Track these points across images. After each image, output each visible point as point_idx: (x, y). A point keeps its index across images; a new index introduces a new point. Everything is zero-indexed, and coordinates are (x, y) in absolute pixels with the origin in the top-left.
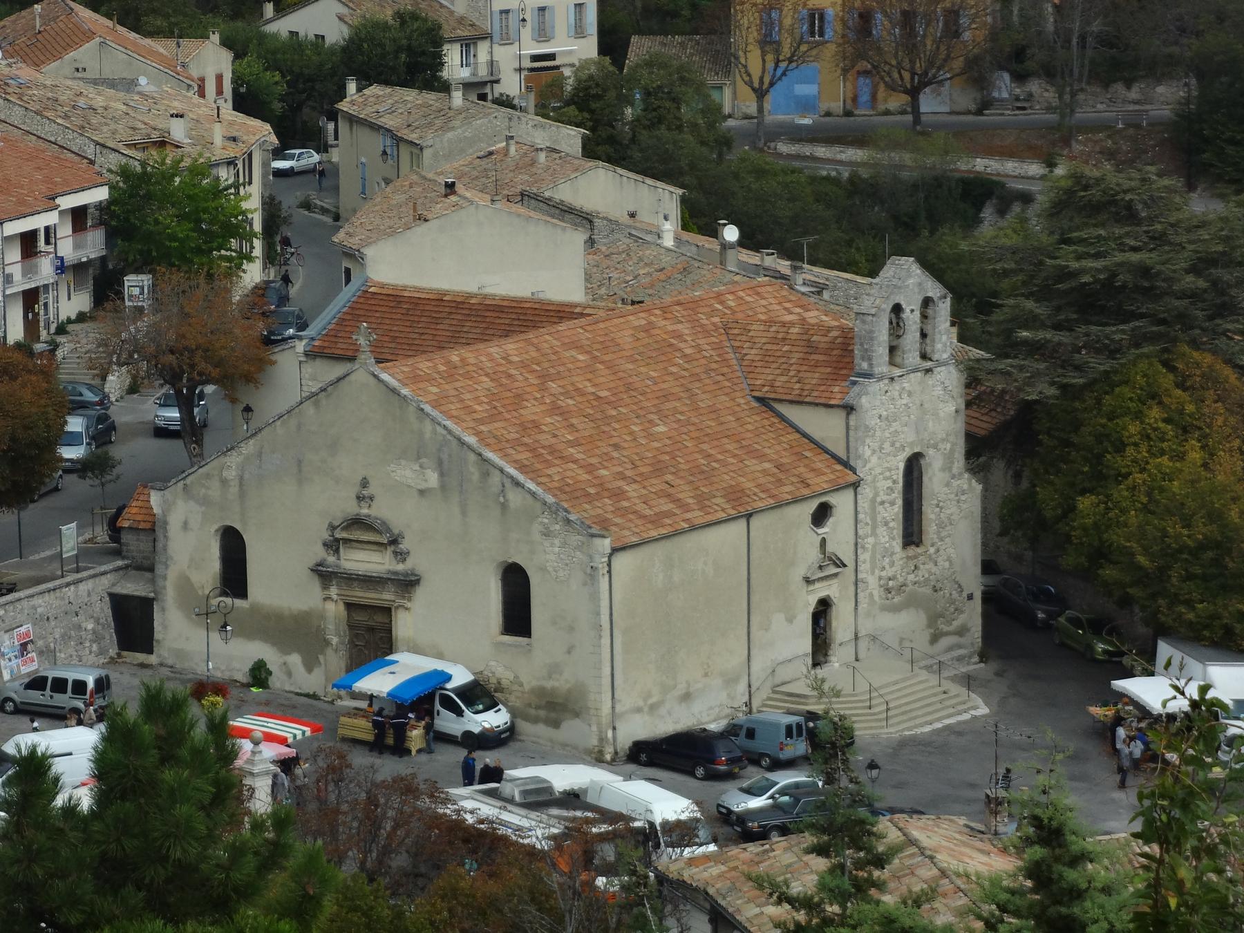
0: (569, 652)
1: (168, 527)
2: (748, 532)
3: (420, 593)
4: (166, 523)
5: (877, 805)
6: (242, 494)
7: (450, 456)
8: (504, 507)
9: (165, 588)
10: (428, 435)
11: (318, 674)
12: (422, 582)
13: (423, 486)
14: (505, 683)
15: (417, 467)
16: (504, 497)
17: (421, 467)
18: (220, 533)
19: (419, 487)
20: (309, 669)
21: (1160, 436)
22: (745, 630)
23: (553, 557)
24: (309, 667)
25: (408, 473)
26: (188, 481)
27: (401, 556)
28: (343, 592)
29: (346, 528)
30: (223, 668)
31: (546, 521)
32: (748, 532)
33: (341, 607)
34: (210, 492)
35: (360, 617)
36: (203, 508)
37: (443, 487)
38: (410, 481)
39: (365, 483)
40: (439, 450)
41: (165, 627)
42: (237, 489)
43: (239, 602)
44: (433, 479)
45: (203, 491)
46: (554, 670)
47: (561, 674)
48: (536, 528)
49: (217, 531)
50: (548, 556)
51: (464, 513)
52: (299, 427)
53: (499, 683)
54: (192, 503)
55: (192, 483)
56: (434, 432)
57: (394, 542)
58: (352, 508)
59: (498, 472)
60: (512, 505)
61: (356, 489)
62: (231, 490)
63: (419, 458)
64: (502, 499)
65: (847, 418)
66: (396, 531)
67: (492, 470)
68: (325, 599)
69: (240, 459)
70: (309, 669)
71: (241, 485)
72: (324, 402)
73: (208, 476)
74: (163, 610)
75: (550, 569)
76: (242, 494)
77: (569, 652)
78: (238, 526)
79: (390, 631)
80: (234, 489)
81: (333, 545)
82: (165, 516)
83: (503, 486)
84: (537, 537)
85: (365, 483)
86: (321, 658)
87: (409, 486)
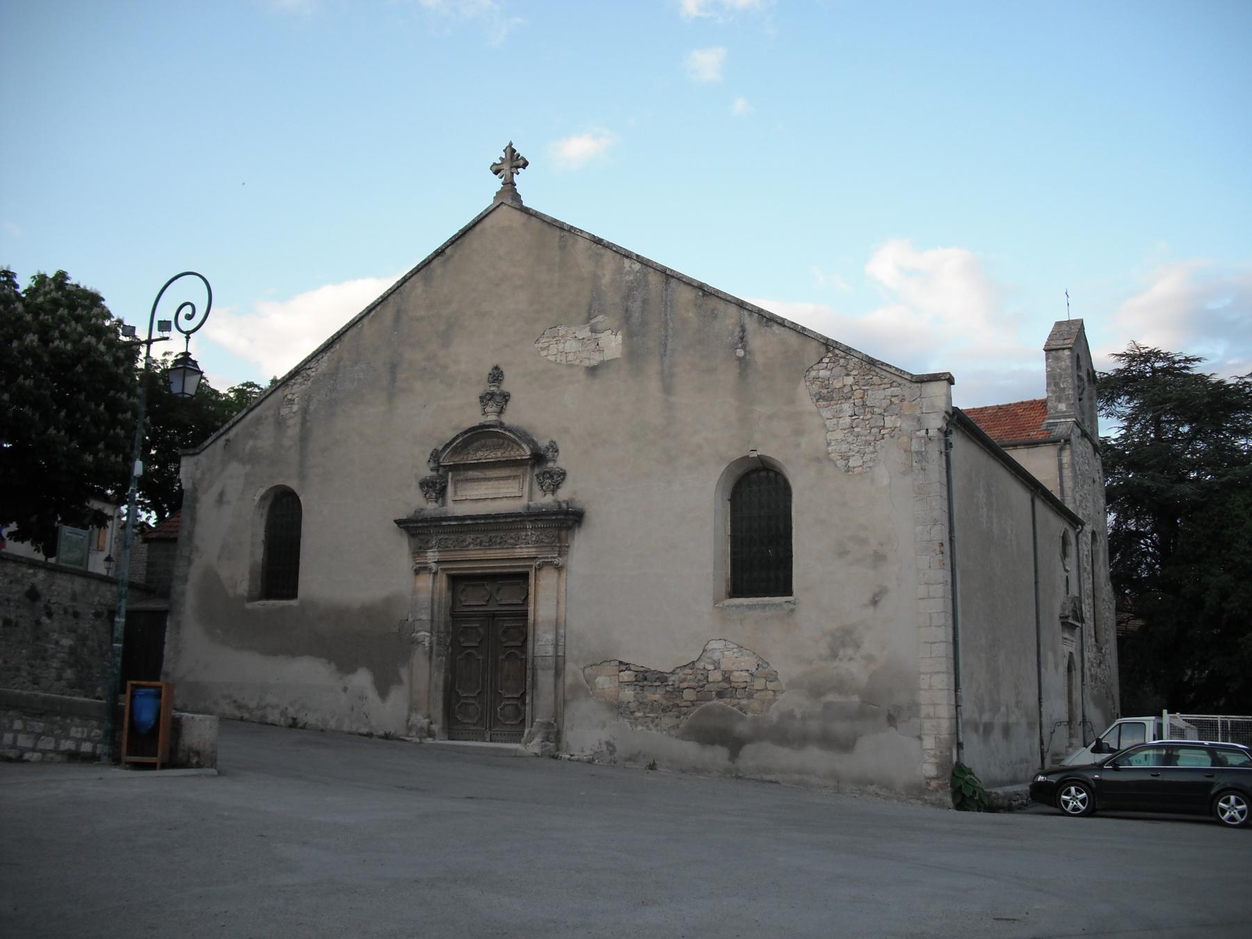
0: (874, 602)
3: (581, 545)
4: (195, 500)
5: (742, 728)
7: (645, 302)
9: (183, 594)
11: (398, 699)
14: (739, 677)
17: (593, 331)
18: (268, 503)
19: (586, 363)
20: (383, 693)
22: (1041, 607)
23: (839, 435)
24: (383, 687)
26: (232, 434)
27: (556, 479)
28: (449, 556)
29: (456, 451)
33: (443, 582)
37: (633, 354)
39: (497, 375)
40: (628, 297)
43: (293, 603)
44: (613, 344)
46: (844, 639)
47: (858, 647)
48: (804, 393)
49: (263, 498)
50: (830, 436)
51: (668, 389)
56: (620, 270)
57: (538, 458)
58: (474, 417)
59: (733, 309)
61: (484, 387)
63: (589, 318)
64: (740, 353)
65: (1059, 455)
66: (543, 443)
67: (721, 306)
68: (417, 572)
70: (383, 693)
71: (304, 422)
72: (439, 271)
74: (178, 625)
77: (874, 602)
79: (525, 615)
81: (435, 487)
82: (195, 489)
83: (743, 330)
84: (808, 404)
85: (497, 375)
86: (404, 673)
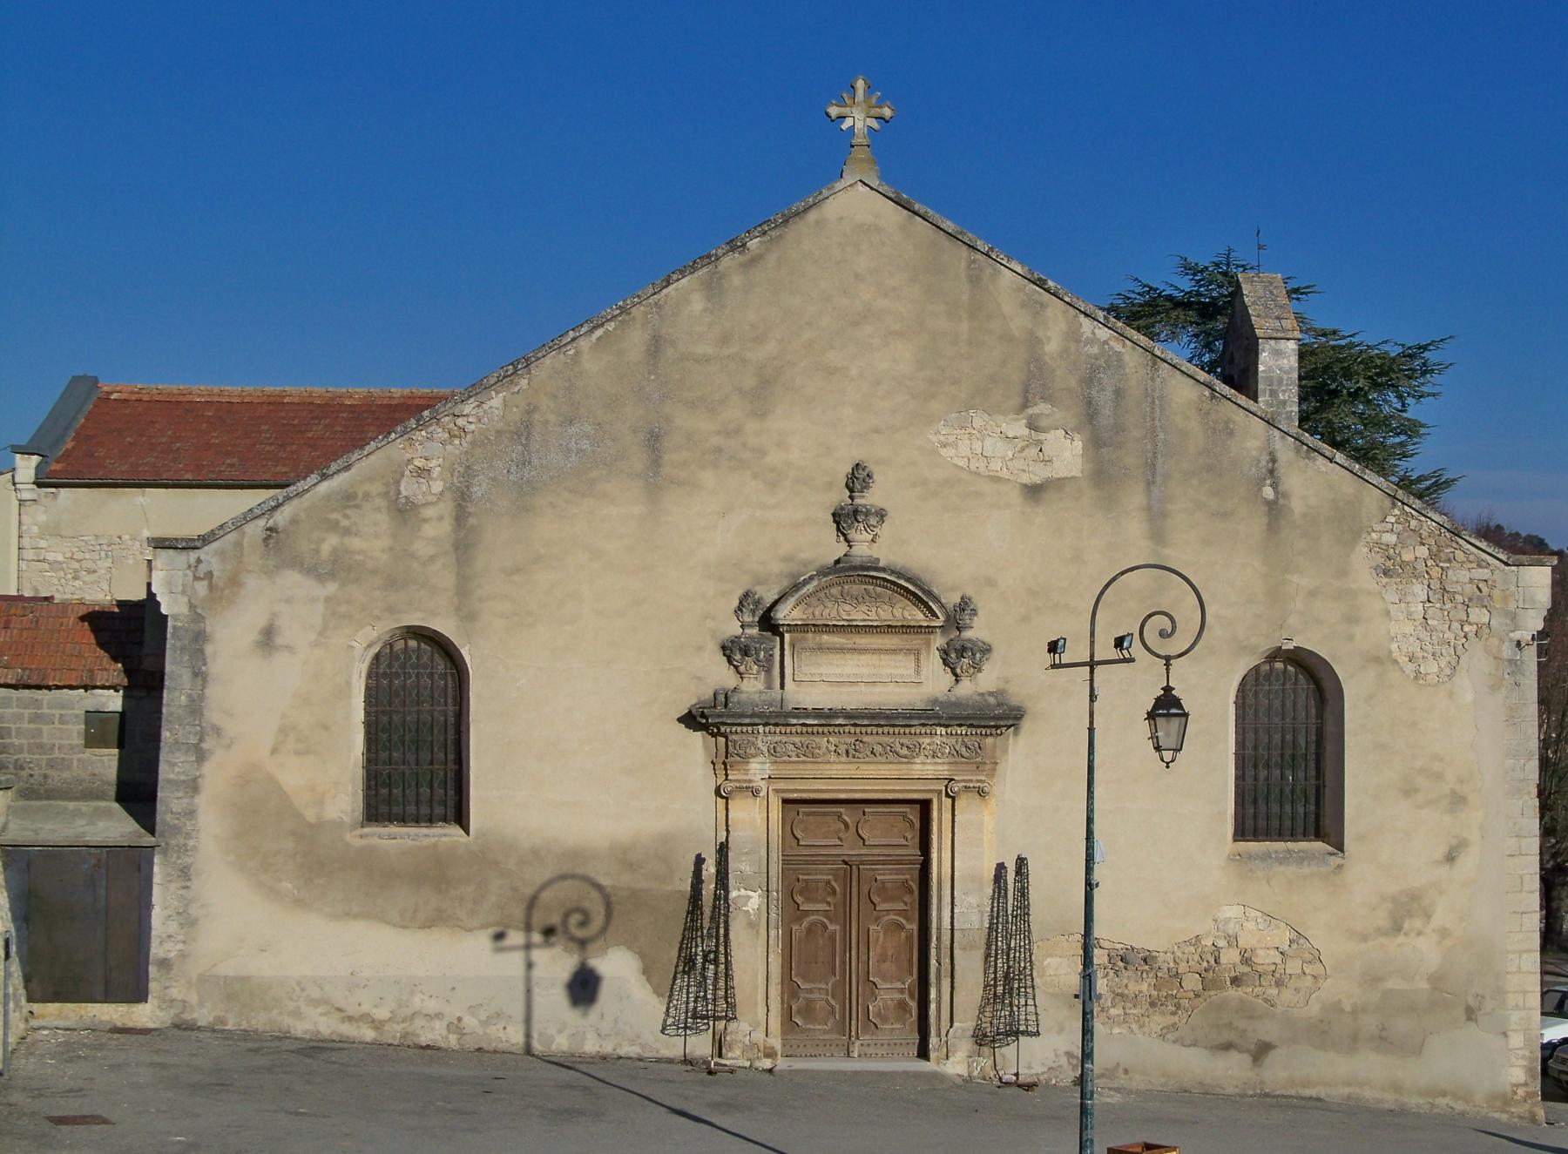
0: (1450, 858)
1: (209, 649)
2: (1090, 821)
4: (200, 638)
6: (463, 546)
7: (1118, 393)
8: (1275, 510)
10: (1052, 346)
12: (1026, 725)
13: (1038, 474)
15: (1019, 428)
16: (1275, 486)
17: (1032, 426)
21: (739, 612)
25: (992, 445)
30: (382, 1014)
31: (1391, 539)
32: (1090, 821)
34: (355, 543)
35: (823, 837)
36: (332, 588)
37: (1102, 475)
38: (996, 465)
39: (858, 479)
41: (189, 922)
42: (447, 526)
45: (332, 541)
48: (1362, 560)
52: (656, 347)
53: (1246, 961)
54: (292, 579)
55: (294, 521)
60: (1297, 506)
62: (429, 530)
63: (1025, 405)
64: (1268, 492)
69: (457, 447)
71: (460, 517)
73: (348, 499)
74: (185, 873)
75: (1403, 660)
76: (463, 546)
77: (1450, 858)
78: (445, 626)
80: (436, 527)
85: (858, 479)
87: (996, 479)
